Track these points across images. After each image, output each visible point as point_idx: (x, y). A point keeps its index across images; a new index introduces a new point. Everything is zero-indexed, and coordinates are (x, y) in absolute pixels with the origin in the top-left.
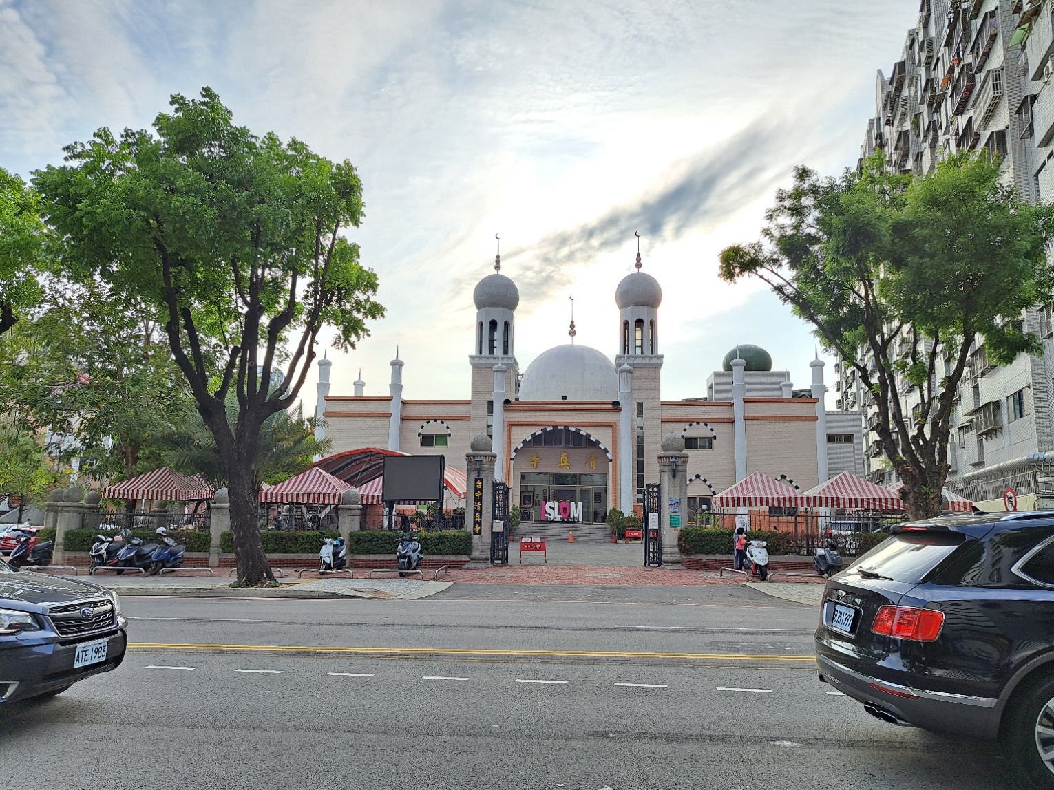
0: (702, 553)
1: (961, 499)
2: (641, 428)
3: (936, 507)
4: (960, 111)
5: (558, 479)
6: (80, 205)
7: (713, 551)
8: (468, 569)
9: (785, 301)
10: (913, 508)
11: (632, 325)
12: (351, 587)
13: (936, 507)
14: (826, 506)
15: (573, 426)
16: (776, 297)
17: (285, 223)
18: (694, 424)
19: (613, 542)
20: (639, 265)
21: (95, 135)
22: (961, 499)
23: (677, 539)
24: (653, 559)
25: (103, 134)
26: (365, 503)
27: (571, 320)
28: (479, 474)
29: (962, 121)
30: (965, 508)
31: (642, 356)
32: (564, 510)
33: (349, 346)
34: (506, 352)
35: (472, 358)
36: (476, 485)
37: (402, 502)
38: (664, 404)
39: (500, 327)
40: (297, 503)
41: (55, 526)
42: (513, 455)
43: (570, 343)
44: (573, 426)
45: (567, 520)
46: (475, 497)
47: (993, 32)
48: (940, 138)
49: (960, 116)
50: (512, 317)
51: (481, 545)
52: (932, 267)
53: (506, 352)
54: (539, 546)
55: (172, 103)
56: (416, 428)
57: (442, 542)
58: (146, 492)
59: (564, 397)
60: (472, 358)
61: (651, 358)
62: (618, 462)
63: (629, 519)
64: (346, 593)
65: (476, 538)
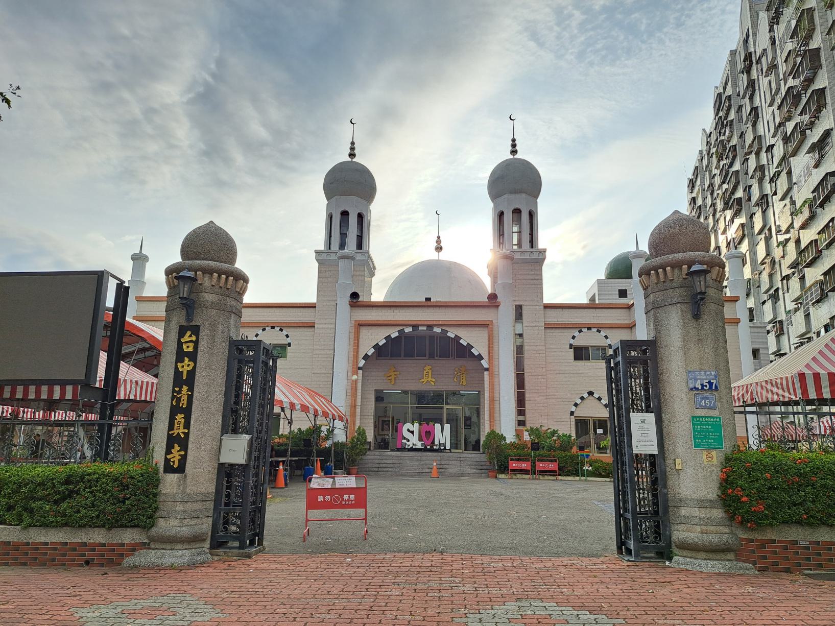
0: (799, 523)
2: (521, 335)
5: (421, 397)
8: (135, 567)
11: (508, 217)
15: (438, 325)
18: (585, 330)
19: (492, 477)
20: (514, 152)
28: (189, 317)
31: (520, 250)
32: (427, 435)
34: (360, 246)
35: (318, 252)
36: (180, 344)
38: (548, 307)
39: (353, 220)
42: (362, 363)
43: (437, 259)
44: (438, 325)
45: (430, 448)
46: (178, 374)
50: (368, 209)
53: (360, 246)
54: (352, 497)
59: (428, 299)
60: (318, 252)
61: (532, 252)
62: (496, 371)
63: (513, 446)
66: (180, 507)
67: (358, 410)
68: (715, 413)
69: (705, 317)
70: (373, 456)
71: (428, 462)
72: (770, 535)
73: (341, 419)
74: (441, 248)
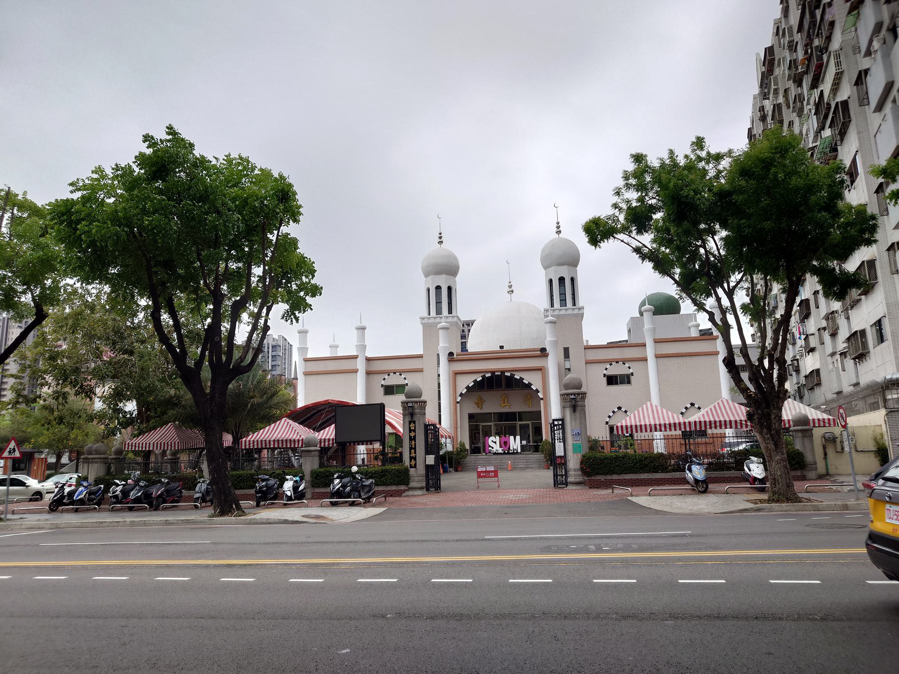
0: (600, 474)
1: (826, 416)
3: (777, 424)
4: (814, 85)
6: (79, 226)
7: (609, 472)
9: (643, 260)
10: (758, 427)
12: (303, 514)
13: (777, 424)
14: (731, 427)
15: (508, 371)
16: (636, 256)
17: (236, 226)
21: (93, 172)
22: (826, 416)
23: (579, 464)
24: (560, 482)
25: (99, 170)
26: (322, 445)
27: (508, 281)
28: (412, 417)
29: (816, 93)
30: (829, 424)
32: (505, 444)
33: (294, 320)
36: (410, 427)
37: (369, 443)
38: (588, 348)
40: (287, 448)
41: (88, 474)
42: (459, 399)
44: (508, 371)
45: (508, 452)
46: (410, 437)
47: (831, 20)
48: (805, 108)
49: (816, 90)
51: (417, 475)
52: (749, 226)
55: (144, 142)
56: (381, 381)
57: (385, 475)
58: (155, 444)
59: (502, 347)
64: (300, 520)
65: (412, 471)
66: (416, 478)
67: (459, 430)
68: (579, 442)
69: (577, 411)
70: (471, 459)
71: (505, 461)
72: (593, 478)
73: (450, 437)
74: (512, 291)
